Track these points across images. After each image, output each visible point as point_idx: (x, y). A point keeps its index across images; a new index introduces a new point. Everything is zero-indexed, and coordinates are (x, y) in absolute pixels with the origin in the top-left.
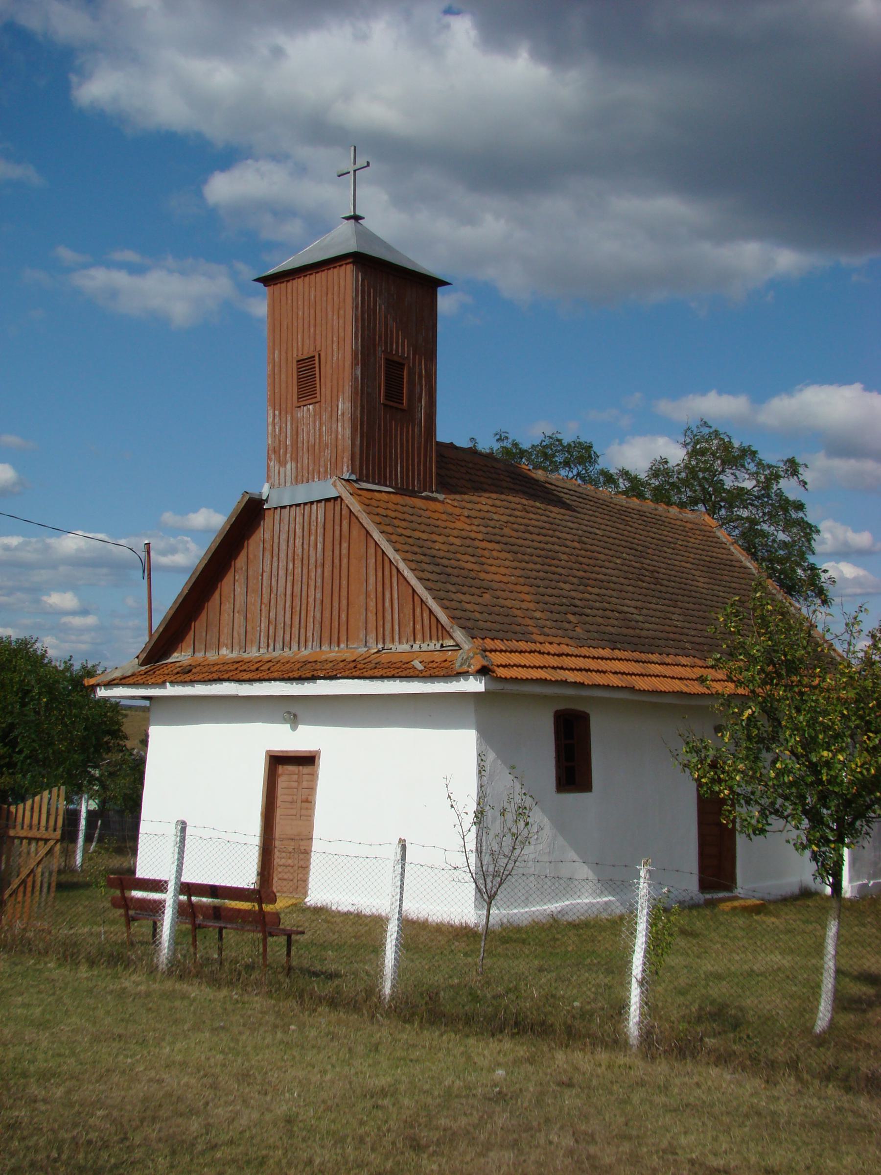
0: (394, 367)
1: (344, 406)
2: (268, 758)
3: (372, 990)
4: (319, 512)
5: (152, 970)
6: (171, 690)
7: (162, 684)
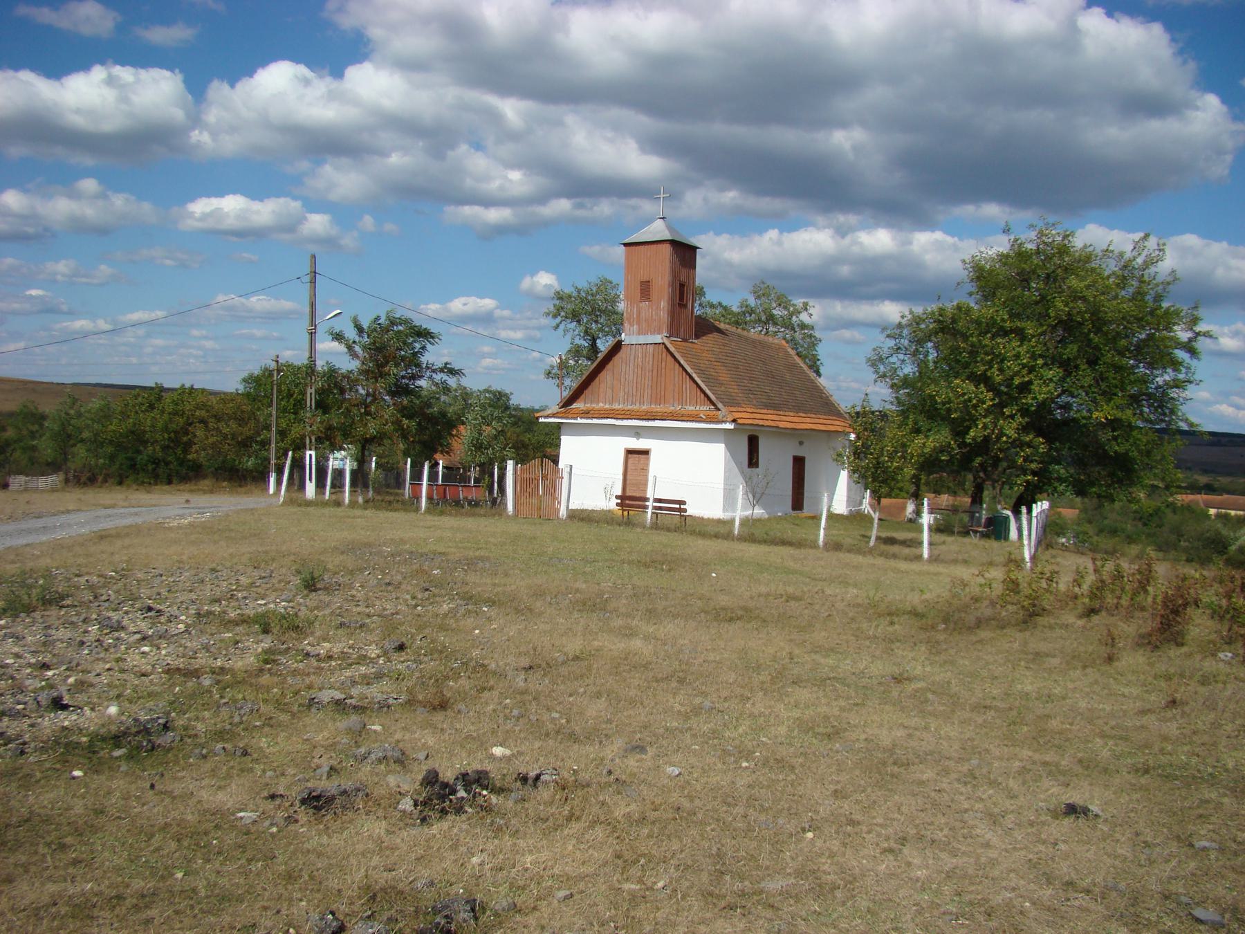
0: (682, 286)
1: (664, 304)
3: (731, 532)
4: (651, 348)
5: (644, 527)
6: (579, 421)
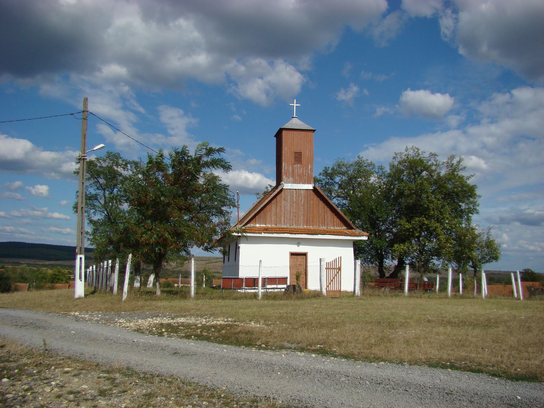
6: (263, 235)
7: (261, 233)
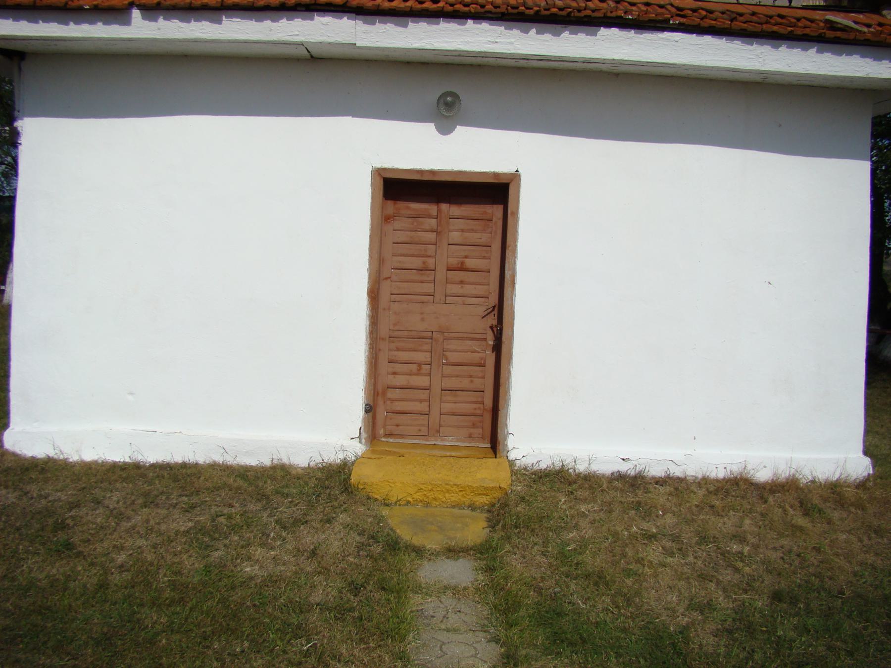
2: (380, 184)
